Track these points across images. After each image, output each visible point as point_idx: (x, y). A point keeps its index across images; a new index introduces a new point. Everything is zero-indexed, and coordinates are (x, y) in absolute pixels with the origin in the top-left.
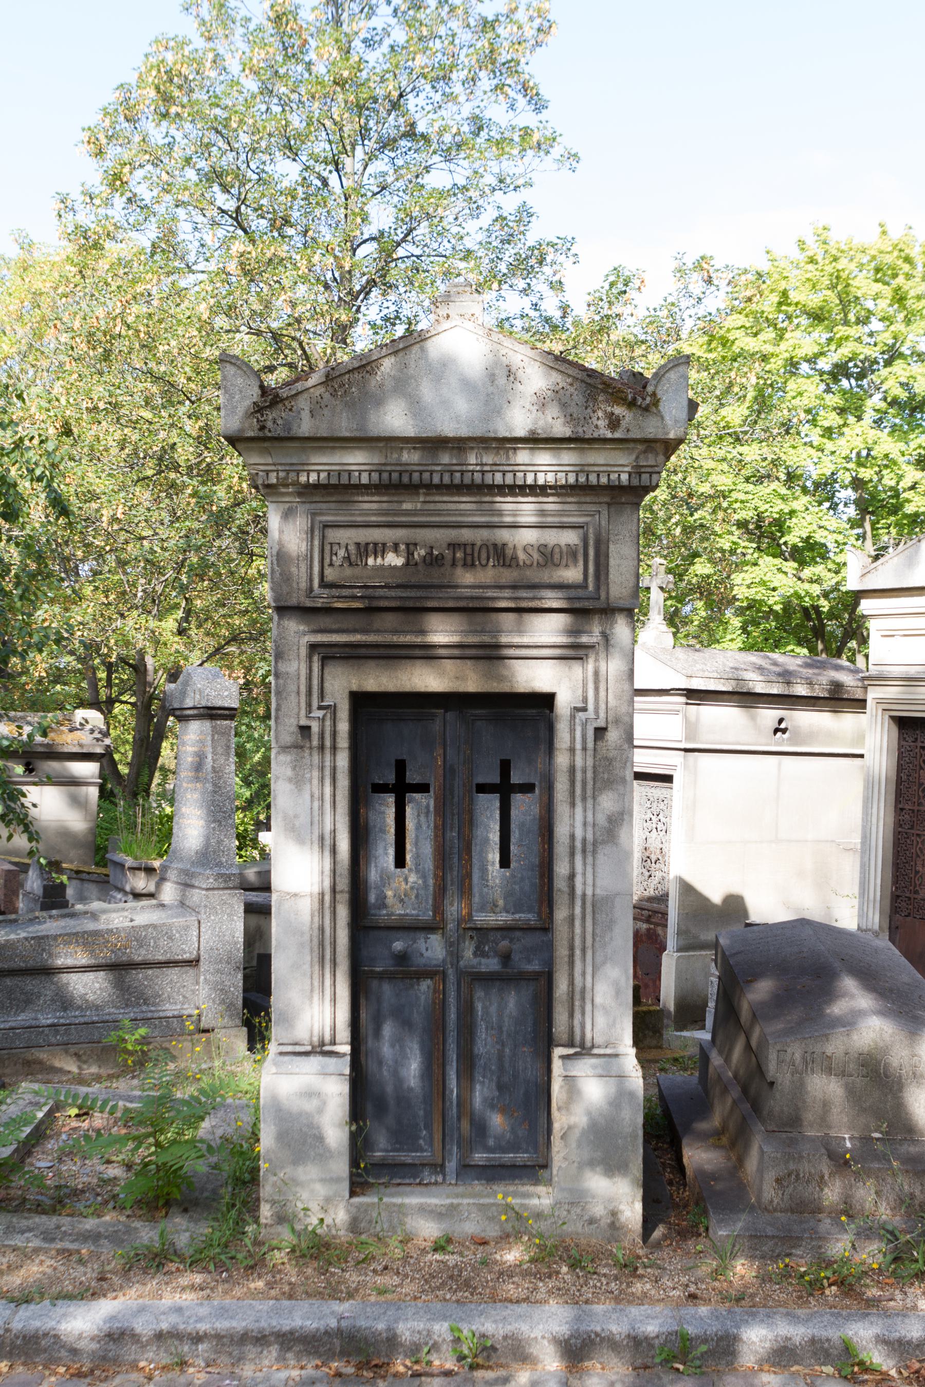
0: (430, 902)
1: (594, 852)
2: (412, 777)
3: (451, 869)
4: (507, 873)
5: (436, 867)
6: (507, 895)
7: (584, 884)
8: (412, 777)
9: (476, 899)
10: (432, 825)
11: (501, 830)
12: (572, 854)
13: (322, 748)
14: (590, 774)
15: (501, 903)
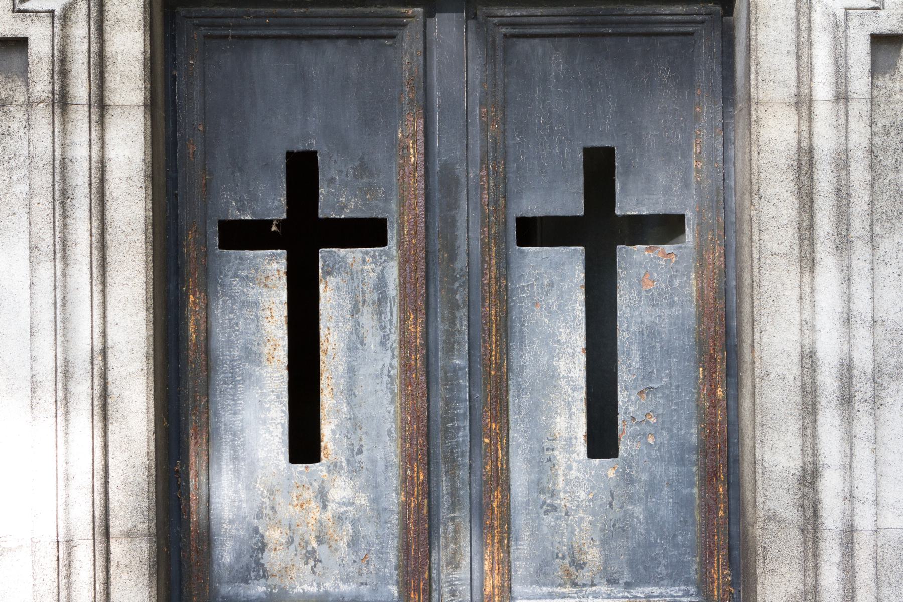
0: (393, 557)
1: (876, 403)
2: (336, 200)
3: (451, 461)
4: (607, 468)
5: (408, 459)
6: (613, 532)
7: (850, 497)
8: (336, 200)
9: (523, 550)
10: (395, 337)
11: (591, 350)
12: (810, 408)
13: (61, 101)
14: (859, 173)
15: (593, 555)
